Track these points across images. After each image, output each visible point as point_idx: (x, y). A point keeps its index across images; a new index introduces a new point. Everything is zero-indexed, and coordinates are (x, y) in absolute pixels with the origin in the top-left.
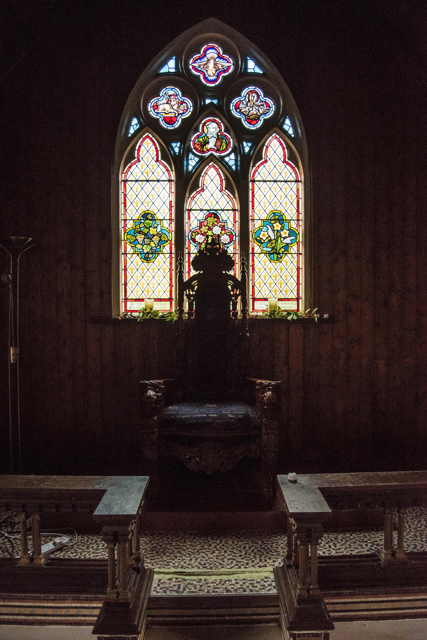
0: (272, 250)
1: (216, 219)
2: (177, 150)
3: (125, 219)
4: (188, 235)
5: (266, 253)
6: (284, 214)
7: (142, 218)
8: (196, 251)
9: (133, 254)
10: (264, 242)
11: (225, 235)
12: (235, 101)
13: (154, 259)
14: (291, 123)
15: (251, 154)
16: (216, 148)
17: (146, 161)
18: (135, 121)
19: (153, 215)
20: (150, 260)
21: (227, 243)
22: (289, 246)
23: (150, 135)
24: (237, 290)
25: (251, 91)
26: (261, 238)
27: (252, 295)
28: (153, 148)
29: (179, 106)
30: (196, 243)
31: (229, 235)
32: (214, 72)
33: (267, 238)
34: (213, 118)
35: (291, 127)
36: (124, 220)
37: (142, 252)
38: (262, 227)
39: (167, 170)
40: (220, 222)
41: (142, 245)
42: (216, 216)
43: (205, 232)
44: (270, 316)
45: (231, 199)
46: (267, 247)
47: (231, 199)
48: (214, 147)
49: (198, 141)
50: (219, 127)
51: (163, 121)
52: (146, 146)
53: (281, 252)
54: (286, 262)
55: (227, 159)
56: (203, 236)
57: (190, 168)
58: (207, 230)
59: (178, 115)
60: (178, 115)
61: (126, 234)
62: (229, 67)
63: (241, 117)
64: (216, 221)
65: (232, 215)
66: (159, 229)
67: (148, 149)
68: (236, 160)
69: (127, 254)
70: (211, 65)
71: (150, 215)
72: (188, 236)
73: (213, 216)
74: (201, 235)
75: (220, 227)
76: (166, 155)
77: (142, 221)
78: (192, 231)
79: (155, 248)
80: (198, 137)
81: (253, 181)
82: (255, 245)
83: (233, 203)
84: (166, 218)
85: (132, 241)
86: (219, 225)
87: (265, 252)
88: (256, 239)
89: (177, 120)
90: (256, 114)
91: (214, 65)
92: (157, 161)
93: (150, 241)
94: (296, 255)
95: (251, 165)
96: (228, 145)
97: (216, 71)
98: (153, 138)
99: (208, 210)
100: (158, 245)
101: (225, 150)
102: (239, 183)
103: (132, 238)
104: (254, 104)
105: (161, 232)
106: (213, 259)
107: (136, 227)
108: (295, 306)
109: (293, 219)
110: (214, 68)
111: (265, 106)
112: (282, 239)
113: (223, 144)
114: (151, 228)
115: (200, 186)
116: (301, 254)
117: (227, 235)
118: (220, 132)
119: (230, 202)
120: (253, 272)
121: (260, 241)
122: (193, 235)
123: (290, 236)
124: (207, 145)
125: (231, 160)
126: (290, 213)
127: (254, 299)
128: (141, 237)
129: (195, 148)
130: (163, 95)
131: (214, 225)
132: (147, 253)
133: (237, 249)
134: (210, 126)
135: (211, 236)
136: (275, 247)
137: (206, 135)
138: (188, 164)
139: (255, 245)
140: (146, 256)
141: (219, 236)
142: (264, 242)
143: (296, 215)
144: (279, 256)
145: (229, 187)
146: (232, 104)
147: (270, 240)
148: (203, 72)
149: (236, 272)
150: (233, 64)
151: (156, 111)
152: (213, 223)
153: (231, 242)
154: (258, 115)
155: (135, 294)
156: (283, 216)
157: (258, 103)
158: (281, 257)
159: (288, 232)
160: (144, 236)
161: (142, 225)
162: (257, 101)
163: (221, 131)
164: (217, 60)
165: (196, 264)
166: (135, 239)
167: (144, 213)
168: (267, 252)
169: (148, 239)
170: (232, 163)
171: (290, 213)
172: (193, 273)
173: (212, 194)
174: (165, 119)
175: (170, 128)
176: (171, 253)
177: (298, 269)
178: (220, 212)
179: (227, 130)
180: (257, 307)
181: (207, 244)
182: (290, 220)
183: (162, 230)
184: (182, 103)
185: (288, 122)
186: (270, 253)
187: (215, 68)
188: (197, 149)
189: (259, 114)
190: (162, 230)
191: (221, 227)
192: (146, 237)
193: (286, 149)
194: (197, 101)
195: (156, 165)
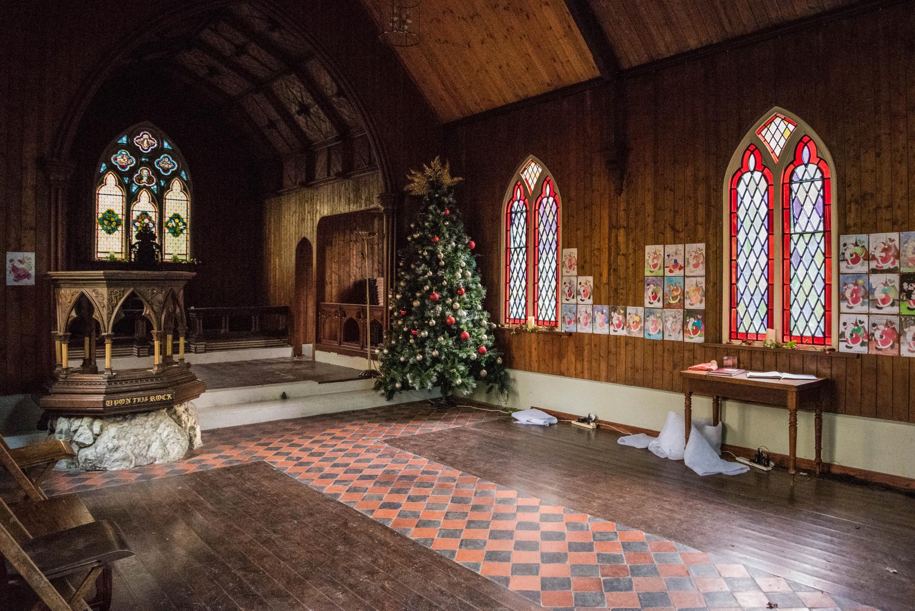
67: (111, 179)
76: (120, 184)
102: (158, 199)
106: (145, 235)
126: (183, 215)
145: (153, 201)
149: (157, 241)
173: (144, 203)
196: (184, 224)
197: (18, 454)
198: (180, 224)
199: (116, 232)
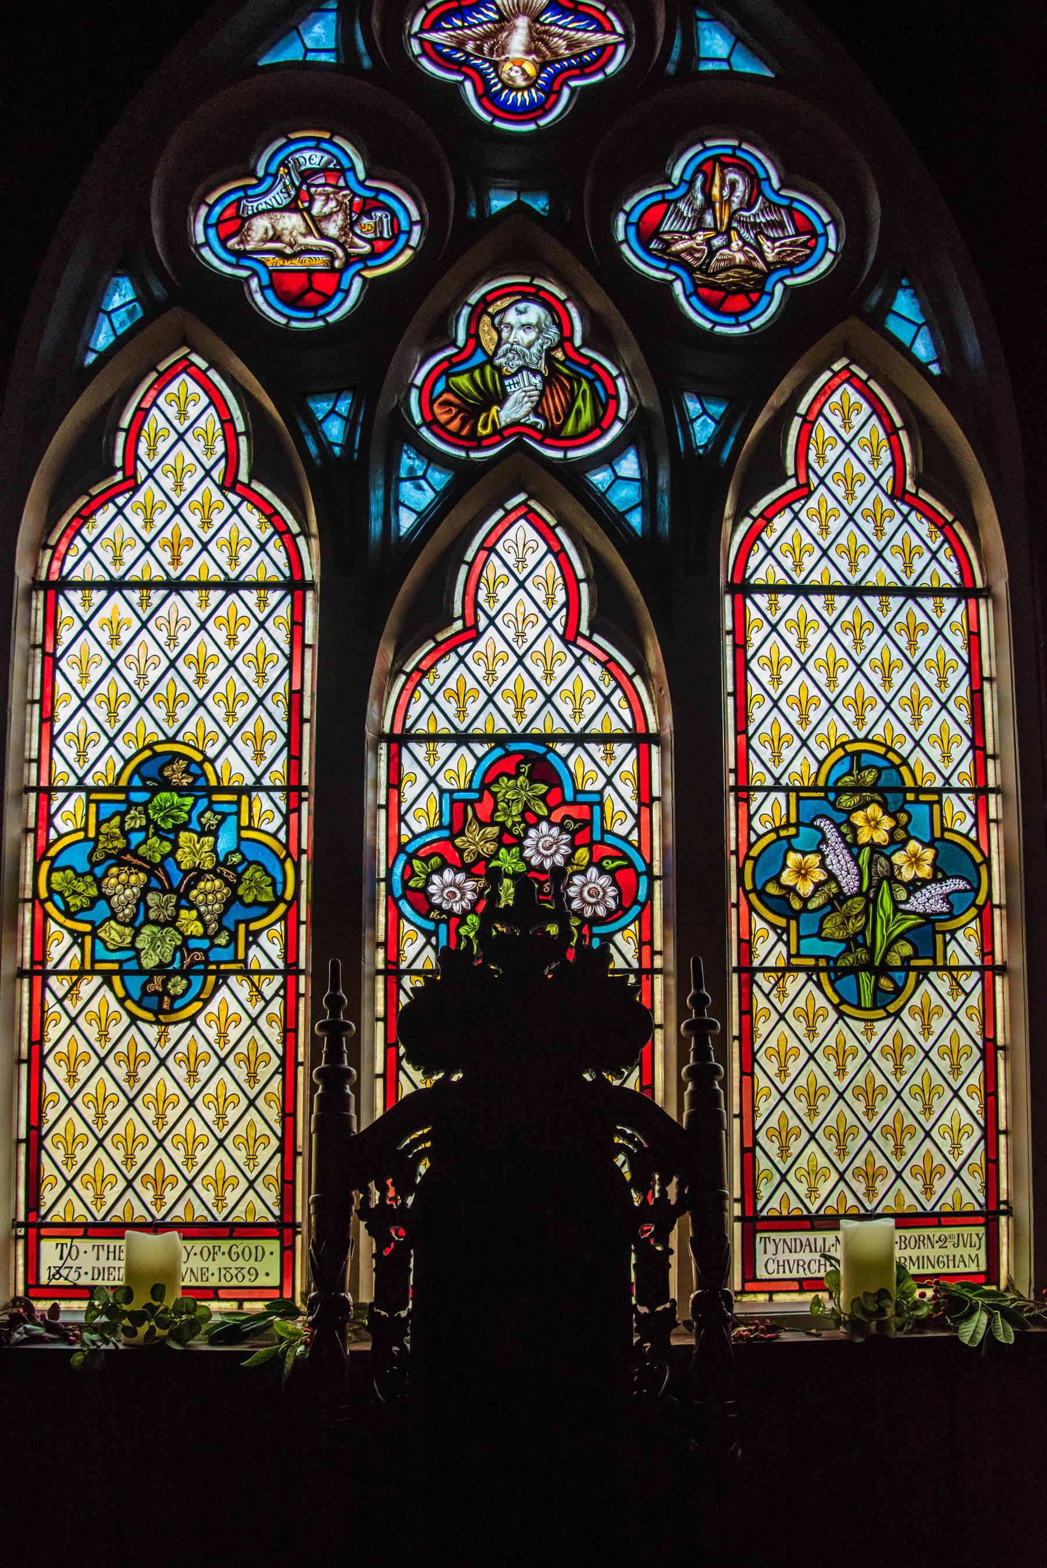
0: (848, 950)
1: (542, 788)
2: (335, 430)
3: (44, 783)
4: (390, 871)
5: (816, 969)
6: (905, 762)
7: (137, 782)
8: (428, 960)
9: (81, 973)
10: (805, 909)
11: (593, 872)
12: (637, 202)
13: (198, 1005)
14: (923, 311)
15: (725, 455)
16: (542, 424)
17: (168, 483)
18: (121, 295)
19: (196, 768)
20: (172, 1011)
21: (601, 911)
22: (939, 927)
23: (195, 358)
24: (665, 1182)
25: (716, 159)
26: (792, 889)
27: (741, 1200)
28: (211, 420)
29: (353, 224)
30: (433, 914)
31: (612, 873)
32: (531, 70)
33: (818, 886)
34: (526, 280)
35: (924, 330)
36: (38, 789)
37: (132, 965)
38: (792, 831)
39: (282, 531)
40: (564, 803)
41: (130, 924)
42: (543, 771)
43: (480, 858)
44: (856, 1325)
45: (624, 680)
46: (818, 935)
47: (624, 680)
48: (533, 419)
49: (448, 389)
50: (563, 324)
51: (269, 294)
52: (172, 412)
53: (895, 960)
54: (926, 1015)
55: (600, 478)
56: (470, 876)
57: (406, 520)
58: (491, 847)
59: (347, 265)
60: (347, 265)
61: (45, 866)
62: (605, 52)
63: (669, 277)
64: (543, 798)
65: (630, 765)
66: (226, 842)
67: (183, 426)
68: (647, 483)
69: (46, 974)
70: (518, 40)
71: (183, 764)
72: (388, 880)
73: (525, 768)
74: (457, 870)
75: (563, 829)
76: (272, 461)
77: (138, 797)
78: (410, 849)
79: (205, 944)
80: (446, 370)
81: (743, 589)
82: (759, 924)
83: (633, 702)
84: (266, 782)
85: (75, 902)
86: (557, 816)
87: (811, 962)
88: (761, 894)
89: (338, 289)
90: (748, 265)
91: (532, 39)
92: (230, 484)
93: (178, 907)
94: (975, 975)
95: (728, 510)
96: (605, 407)
97: (542, 67)
98: (214, 376)
99: (498, 740)
100: (222, 928)
101: (588, 430)
102: (665, 601)
103: (81, 887)
104: (731, 218)
105: (236, 858)
107: (104, 828)
108: (973, 1252)
109: (955, 783)
110: (528, 52)
111: (791, 230)
112: (902, 895)
113: (579, 402)
114: (183, 836)
115: (458, 611)
116: (1002, 970)
117: (602, 871)
118: (560, 345)
119: (617, 697)
120: (747, 1072)
121: (782, 904)
122: (414, 874)
123: (940, 873)
124: (495, 408)
125: (621, 484)
126: (938, 753)
127: (755, 1223)
128: (127, 885)
129: (432, 423)
130: (272, 169)
131: (530, 819)
132: (161, 969)
133: (658, 946)
134: (511, 317)
135: (514, 876)
136: (862, 932)
137: (490, 359)
138: (392, 504)
139: (759, 924)
140: (150, 988)
141: (559, 875)
142: (805, 909)
143: (966, 766)
144: (884, 982)
145: (613, 619)
146: (621, 219)
147: (840, 898)
148: (475, 68)
149: (661, 1076)
150: (627, 39)
151: (232, 243)
152: (526, 809)
153: (622, 909)
154: (756, 270)
155: (88, 1196)
156: (904, 769)
157: (756, 214)
158: (898, 991)
159: (929, 854)
160: (142, 876)
161: (136, 820)
162: (750, 206)
163: (571, 339)
164: (548, 18)
165: (419, 1030)
166: (93, 892)
167: (148, 753)
168: (822, 963)
169: (164, 891)
170: (624, 496)
171: (938, 753)
172: (412, 1080)
173: (522, 649)
174: (276, 282)
175: (304, 324)
176: (291, 971)
177: (989, 1051)
178: (563, 749)
179: (598, 336)
180: (772, 1267)
181: (490, 914)
182: (939, 791)
183: (244, 845)
184: (368, 208)
185: (904, 303)
186: (836, 969)
187: (536, 51)
188: (443, 427)
189: (760, 265)
190: (244, 845)
191: (572, 826)
192: (154, 883)
193: (903, 435)
194: (445, 196)
195: (221, 504)
196: (625, 877)
197: (1028, 1318)
198: (913, 861)
199: (232, 998)
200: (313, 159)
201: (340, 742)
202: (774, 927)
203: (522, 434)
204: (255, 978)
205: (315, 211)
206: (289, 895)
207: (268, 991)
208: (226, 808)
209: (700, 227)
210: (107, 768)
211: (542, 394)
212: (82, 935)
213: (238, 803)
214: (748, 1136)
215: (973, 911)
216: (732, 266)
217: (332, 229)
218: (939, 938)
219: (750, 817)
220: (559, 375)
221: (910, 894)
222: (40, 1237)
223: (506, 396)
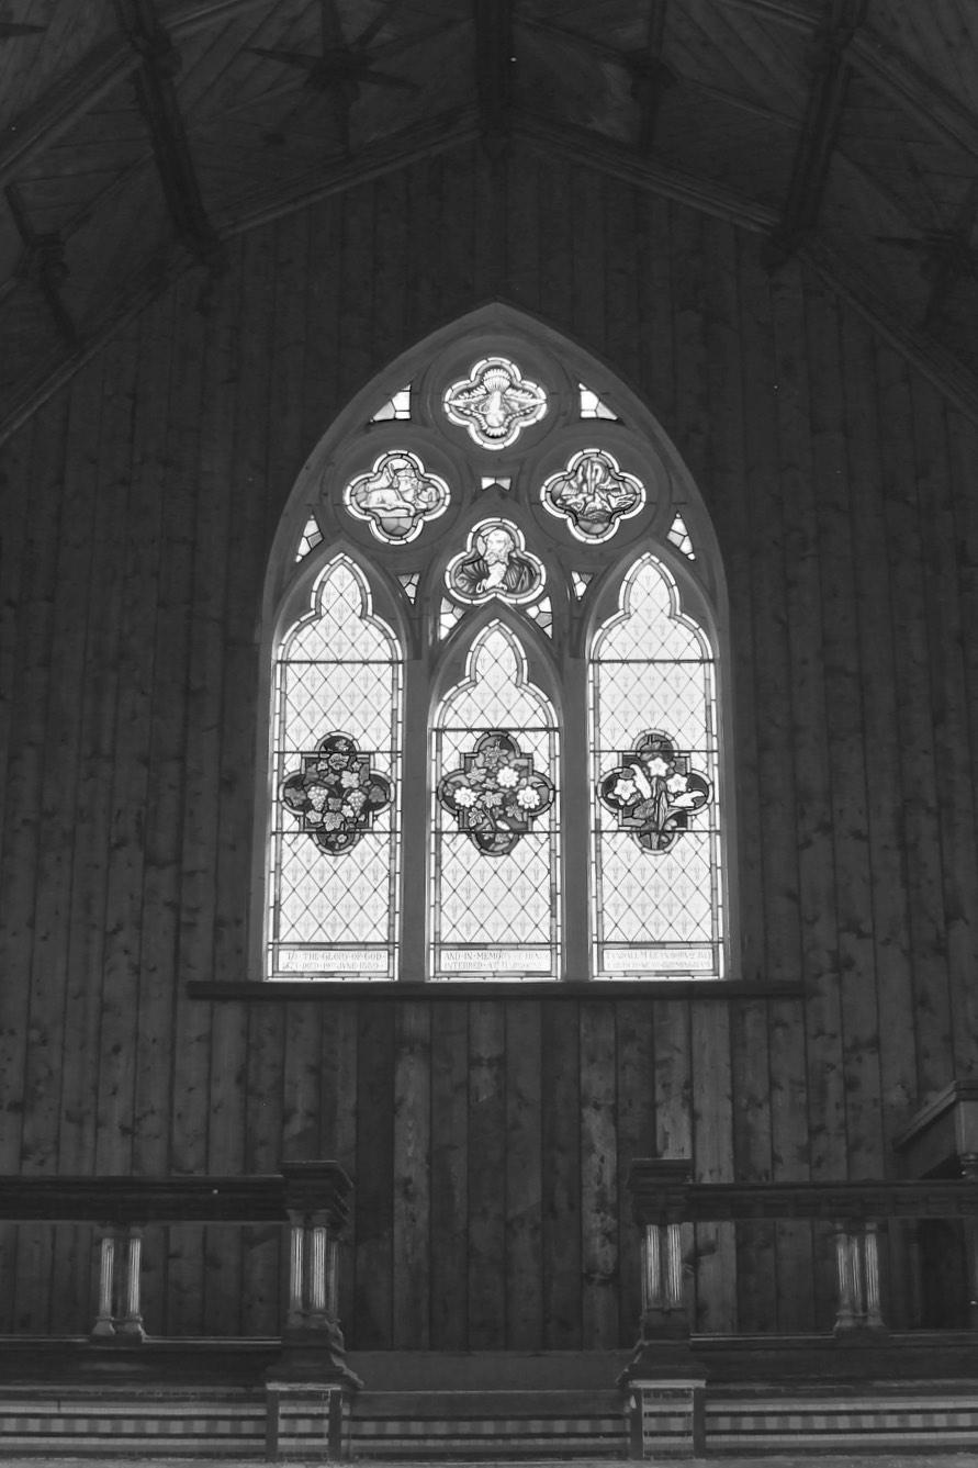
3: (282, 750)
5: (631, 832)
7: (323, 749)
9: (299, 833)
18: (311, 528)
20: (340, 850)
22: (689, 813)
26: (620, 796)
29: (418, 494)
33: (632, 795)
35: (687, 538)
36: (279, 753)
43: (478, 782)
45: (543, 704)
48: (501, 585)
52: (337, 584)
55: (532, 612)
58: (483, 778)
70: (495, 402)
71: (344, 741)
84: (381, 749)
87: (628, 829)
90: (603, 510)
99: (486, 731)
102: (560, 662)
104: (596, 486)
111: (624, 492)
113: (523, 576)
115: (467, 673)
118: (514, 550)
119: (540, 711)
120: (599, 878)
128: (319, 795)
134: (492, 537)
138: (437, 624)
142: (626, 805)
146: (543, 489)
150: (547, 401)
157: (608, 485)
158: (670, 841)
162: (604, 481)
164: (510, 392)
170: (544, 621)
173: (496, 687)
178: (515, 734)
187: (504, 408)
189: (609, 509)
199: (367, 844)
200: (399, 463)
201: (416, 736)
202: (612, 813)
203: (496, 593)
204: (377, 835)
205: (401, 489)
206: (392, 800)
207: (542, 840)
208: (364, 761)
209: (581, 491)
210: (310, 744)
211: (506, 574)
212: (299, 816)
213: (369, 758)
214: (600, 906)
215: (705, 806)
216: (595, 510)
217: (409, 497)
218: (689, 818)
219: (600, 764)
220: (515, 563)
221: (675, 798)
222: (279, 950)
223: (489, 574)
